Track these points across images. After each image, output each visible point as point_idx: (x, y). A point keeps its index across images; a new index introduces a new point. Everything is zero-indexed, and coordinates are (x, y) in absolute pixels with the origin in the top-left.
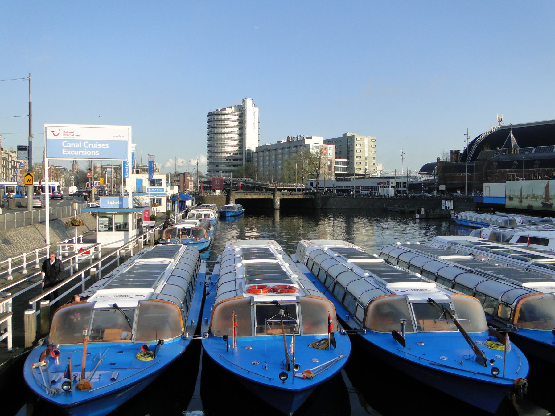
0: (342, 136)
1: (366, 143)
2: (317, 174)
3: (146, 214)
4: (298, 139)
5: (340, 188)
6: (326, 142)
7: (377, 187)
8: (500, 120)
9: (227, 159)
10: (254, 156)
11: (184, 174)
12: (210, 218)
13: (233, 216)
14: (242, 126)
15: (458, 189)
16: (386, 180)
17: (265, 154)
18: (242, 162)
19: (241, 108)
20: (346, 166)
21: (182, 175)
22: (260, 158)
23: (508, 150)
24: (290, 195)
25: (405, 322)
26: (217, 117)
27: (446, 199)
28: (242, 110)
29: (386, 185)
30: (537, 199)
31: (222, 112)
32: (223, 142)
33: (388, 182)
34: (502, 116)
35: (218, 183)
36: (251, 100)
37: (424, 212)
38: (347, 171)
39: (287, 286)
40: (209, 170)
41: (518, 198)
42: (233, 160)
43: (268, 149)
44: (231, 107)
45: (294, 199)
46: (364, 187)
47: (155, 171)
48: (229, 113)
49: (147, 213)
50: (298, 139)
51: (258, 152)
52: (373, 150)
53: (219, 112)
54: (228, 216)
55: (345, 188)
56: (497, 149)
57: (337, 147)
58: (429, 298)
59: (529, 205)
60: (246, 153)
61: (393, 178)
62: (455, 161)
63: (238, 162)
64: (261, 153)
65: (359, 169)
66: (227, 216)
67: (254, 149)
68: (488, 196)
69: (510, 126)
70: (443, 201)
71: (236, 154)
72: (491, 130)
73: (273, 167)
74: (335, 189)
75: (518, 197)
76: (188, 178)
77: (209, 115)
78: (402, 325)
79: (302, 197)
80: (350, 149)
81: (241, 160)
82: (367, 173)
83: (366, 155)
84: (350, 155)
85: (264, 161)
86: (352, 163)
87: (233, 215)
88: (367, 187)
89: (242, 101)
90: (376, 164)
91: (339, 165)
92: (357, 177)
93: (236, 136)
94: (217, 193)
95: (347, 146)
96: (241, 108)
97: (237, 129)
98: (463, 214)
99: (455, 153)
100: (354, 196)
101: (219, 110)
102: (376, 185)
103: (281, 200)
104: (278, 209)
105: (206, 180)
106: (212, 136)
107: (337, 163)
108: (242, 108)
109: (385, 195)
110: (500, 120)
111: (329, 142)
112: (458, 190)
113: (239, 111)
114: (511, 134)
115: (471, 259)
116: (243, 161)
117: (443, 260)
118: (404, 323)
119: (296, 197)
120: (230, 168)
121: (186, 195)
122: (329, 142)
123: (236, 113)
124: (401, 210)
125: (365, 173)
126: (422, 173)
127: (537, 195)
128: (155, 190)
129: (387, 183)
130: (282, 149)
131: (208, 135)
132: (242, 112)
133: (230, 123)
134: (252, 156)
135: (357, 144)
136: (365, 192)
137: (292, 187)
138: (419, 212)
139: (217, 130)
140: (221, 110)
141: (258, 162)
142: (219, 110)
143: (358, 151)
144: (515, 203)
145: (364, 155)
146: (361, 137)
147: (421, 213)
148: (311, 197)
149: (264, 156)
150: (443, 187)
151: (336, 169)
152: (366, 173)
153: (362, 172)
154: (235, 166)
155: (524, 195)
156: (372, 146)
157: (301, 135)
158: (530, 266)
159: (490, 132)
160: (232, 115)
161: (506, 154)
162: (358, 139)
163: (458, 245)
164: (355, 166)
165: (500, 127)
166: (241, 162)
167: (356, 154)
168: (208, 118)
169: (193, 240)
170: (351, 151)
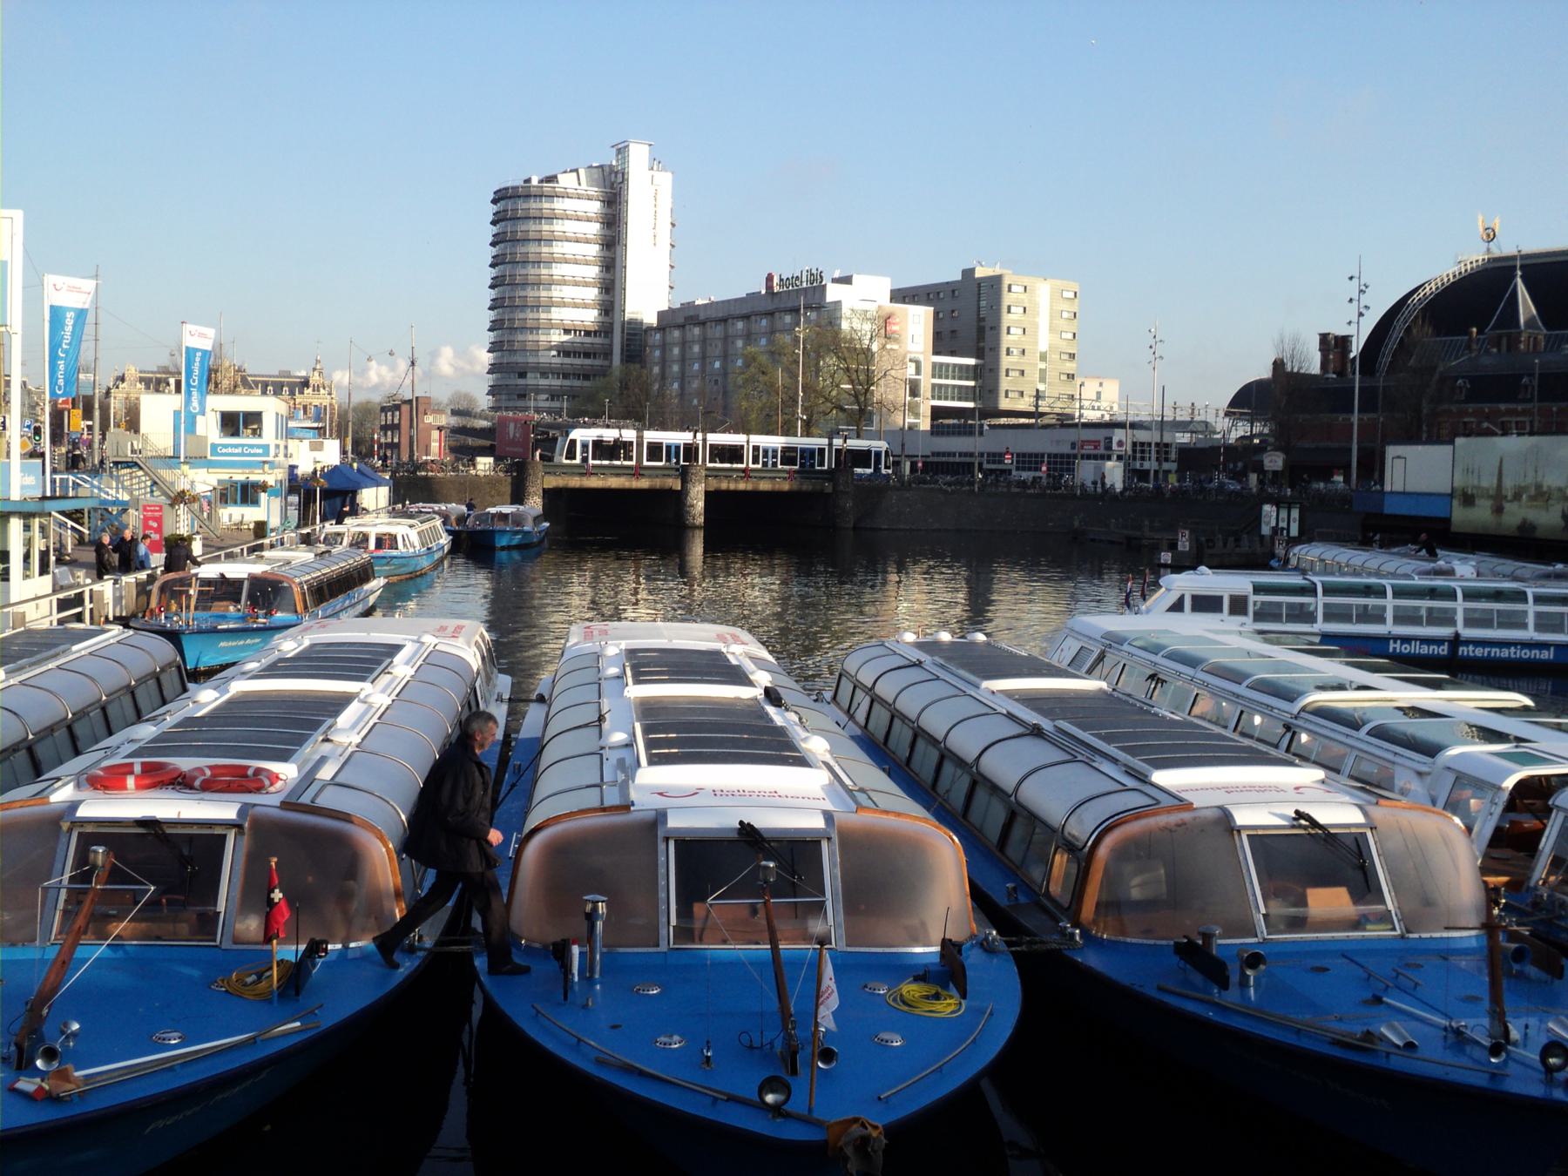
0: (960, 278)
3: (151, 528)
5: (944, 459)
6: (902, 296)
7: (1068, 456)
8: (1491, 236)
9: (564, 350)
10: (650, 341)
12: (397, 549)
13: (518, 547)
15: (1338, 468)
16: (1100, 435)
17: (669, 339)
18: (611, 363)
19: (610, 174)
20: (972, 383)
22: (671, 350)
23: (1509, 336)
25: (602, 908)
26: (525, 206)
27: (1278, 503)
28: (613, 179)
29: (1102, 451)
30: (1550, 502)
33: (1106, 438)
34: (1497, 221)
35: (517, 435)
36: (647, 147)
37: (1187, 543)
39: (248, 767)
40: (494, 391)
41: (1490, 497)
42: (576, 354)
44: (576, 171)
45: (736, 493)
46: (1024, 455)
47: (318, 391)
49: (155, 525)
51: (664, 329)
52: (1069, 329)
53: (534, 187)
54: (503, 548)
55: (963, 459)
56: (1472, 332)
57: (941, 315)
58: (741, 823)
59: (1524, 522)
60: (623, 332)
61: (1121, 425)
62: (1334, 373)
63: (598, 362)
64: (676, 333)
65: (1014, 397)
67: (651, 319)
68: (1401, 489)
69: (1513, 258)
70: (1267, 508)
71: (588, 333)
72: (1456, 268)
73: (716, 381)
75: (1491, 492)
76: (429, 419)
77: (501, 196)
78: (591, 917)
79: (786, 486)
80: (987, 324)
81: (608, 354)
82: (1040, 410)
83: (1043, 347)
85: (683, 360)
87: (514, 542)
88: (1036, 455)
89: (614, 149)
90: (1078, 381)
91: (947, 377)
92: (1003, 421)
94: (480, 467)
96: (610, 174)
97: (597, 247)
98: (1303, 552)
99: (1333, 346)
102: (1066, 449)
103: (710, 496)
104: (698, 527)
105: (484, 424)
106: (507, 269)
107: (938, 370)
108: (613, 175)
109: (1083, 485)
110: (1491, 236)
111: (914, 296)
112: (1335, 471)
114: (1519, 281)
115: (1101, 690)
117: (993, 692)
118: (595, 909)
120: (567, 383)
121: (358, 470)
122: (914, 296)
123: (594, 191)
124: (1129, 539)
126: (1234, 413)
127: (1549, 487)
128: (239, 450)
129: (1102, 444)
130: (746, 317)
131: (493, 266)
132: (612, 188)
133: (570, 227)
134: (645, 341)
135: (1009, 307)
136: (1026, 475)
138: (1173, 546)
140: (541, 181)
141: (664, 362)
142: (535, 182)
143: (1013, 330)
144: (1479, 516)
145: (1036, 343)
147: (1180, 548)
148: (818, 488)
149: (684, 344)
150: (1277, 459)
151: (938, 391)
152: (1037, 406)
153: (1025, 404)
154: (586, 377)
155: (1509, 484)
156: (1065, 315)
157: (814, 271)
158: (1296, 718)
159: (1454, 276)
160: (579, 197)
161: (1499, 350)
162: (1014, 288)
163: (1126, 647)
164: (1005, 383)
165: (1489, 259)
166: (606, 363)
167: (1006, 341)
168: (495, 208)
169: (243, 619)
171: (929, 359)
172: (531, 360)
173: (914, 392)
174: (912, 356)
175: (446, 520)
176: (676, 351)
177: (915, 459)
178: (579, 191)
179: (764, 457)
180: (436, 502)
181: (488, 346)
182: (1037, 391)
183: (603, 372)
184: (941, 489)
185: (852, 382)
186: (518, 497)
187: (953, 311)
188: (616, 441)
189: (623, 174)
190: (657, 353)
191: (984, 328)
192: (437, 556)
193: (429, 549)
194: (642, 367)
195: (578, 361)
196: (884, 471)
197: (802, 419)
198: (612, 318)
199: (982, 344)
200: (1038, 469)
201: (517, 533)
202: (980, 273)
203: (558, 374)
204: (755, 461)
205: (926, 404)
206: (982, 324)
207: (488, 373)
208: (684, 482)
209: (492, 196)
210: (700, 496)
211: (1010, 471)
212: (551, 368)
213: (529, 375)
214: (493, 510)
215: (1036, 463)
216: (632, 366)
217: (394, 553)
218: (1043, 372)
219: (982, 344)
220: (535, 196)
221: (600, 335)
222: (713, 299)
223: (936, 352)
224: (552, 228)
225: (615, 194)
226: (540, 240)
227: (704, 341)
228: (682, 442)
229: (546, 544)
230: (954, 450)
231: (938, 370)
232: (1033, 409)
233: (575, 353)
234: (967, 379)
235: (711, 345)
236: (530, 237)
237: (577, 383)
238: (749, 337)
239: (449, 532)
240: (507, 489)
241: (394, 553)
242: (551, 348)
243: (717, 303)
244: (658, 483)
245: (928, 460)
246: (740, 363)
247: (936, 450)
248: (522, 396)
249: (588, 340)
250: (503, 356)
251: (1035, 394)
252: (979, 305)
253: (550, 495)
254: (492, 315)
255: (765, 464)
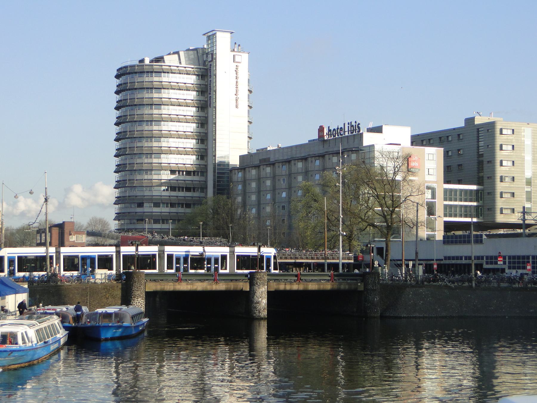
1: (528, 142)
2: (388, 224)
4: (347, 134)
5: (453, 262)
9: (172, 187)
11: (61, 226)
12: (17, 344)
13: (120, 338)
14: (206, 101)
17: (263, 174)
18: (206, 194)
20: (475, 204)
21: (55, 231)
24: (295, 281)
26: (140, 79)
28: (205, 59)
31: (153, 65)
32: (155, 144)
36: (229, 35)
38: (477, 216)
40: (119, 217)
43: (271, 160)
44: (177, 53)
45: (306, 293)
48: (172, 68)
50: (344, 132)
53: (146, 65)
54: (106, 340)
57: (450, 154)
60: (214, 172)
63: (196, 194)
64: (254, 172)
66: (103, 337)
67: (235, 161)
71: (188, 173)
73: (283, 207)
74: (419, 264)
77: (121, 73)
79: (328, 286)
80: (485, 159)
81: (203, 188)
82: (527, 222)
83: (528, 174)
84: (486, 174)
85: (259, 192)
86: (491, 193)
88: (524, 257)
89: (205, 37)
91: (456, 200)
92: (501, 231)
93: (192, 127)
94: (98, 276)
95: (476, 151)
100: (471, 283)
101: (147, 61)
103: (272, 295)
104: (262, 319)
106: (127, 127)
108: (205, 56)
111: (429, 140)
113: (197, 61)
116: (207, 192)
119: (312, 286)
120: (174, 210)
122: (429, 140)
123: (190, 68)
125: (521, 222)
130: (304, 159)
132: (204, 64)
135: (501, 146)
137: (318, 259)
139: (139, 112)
140: (151, 61)
141: (245, 193)
142: (147, 61)
143: (504, 163)
145: (523, 172)
146: (514, 125)
148: (353, 287)
149: (259, 180)
152: (524, 220)
153: (515, 219)
154: (188, 206)
157: (353, 124)
162: (504, 132)
164: (500, 203)
166: (202, 195)
167: (500, 171)
168: (118, 82)
170: (488, 162)
171: (441, 187)
172: (147, 193)
173: (431, 211)
174: (429, 184)
175: (63, 318)
176: (254, 185)
177: (432, 262)
178: (180, 68)
179: (177, 264)
180: (64, 304)
181: (114, 184)
182: (524, 208)
183: (199, 202)
184: (446, 286)
185: (381, 206)
186: (126, 300)
187: (459, 150)
188: (202, 254)
189: (212, 54)
190: (240, 187)
191: (482, 161)
192: (53, 347)
193: (45, 343)
194: (228, 198)
195: (181, 194)
196: (273, 271)
197: (343, 235)
198: (207, 161)
199: (481, 174)
200: (524, 268)
201: (119, 327)
202: (478, 121)
203: (182, 204)
204: (170, 267)
205: (440, 220)
206: (481, 159)
207: (115, 204)
208: (252, 285)
209: (115, 73)
210: (264, 295)
211: (503, 270)
212: (162, 200)
213: (145, 205)
214: (100, 310)
215: (524, 263)
216: (220, 197)
217: (14, 347)
218: (529, 194)
219: (481, 174)
220: (148, 72)
221: (198, 175)
222: (280, 145)
223: (447, 181)
224: (160, 96)
225: (206, 70)
226: (152, 105)
227: (274, 178)
228: (96, 254)
229: (146, 334)
230: (461, 255)
231: (449, 195)
232: (521, 222)
233: (179, 188)
234: (471, 201)
235: (279, 180)
236: (144, 103)
237: (181, 210)
238: (306, 174)
239: (66, 328)
240: (118, 293)
241: (14, 347)
242: (161, 185)
243: (283, 148)
244: (232, 286)
245: (442, 262)
246: (300, 193)
247: (448, 255)
248: (141, 220)
249: (189, 178)
250: (125, 191)
251: (522, 210)
252: (478, 145)
253: (150, 296)
254: (116, 161)
255: (178, 269)
